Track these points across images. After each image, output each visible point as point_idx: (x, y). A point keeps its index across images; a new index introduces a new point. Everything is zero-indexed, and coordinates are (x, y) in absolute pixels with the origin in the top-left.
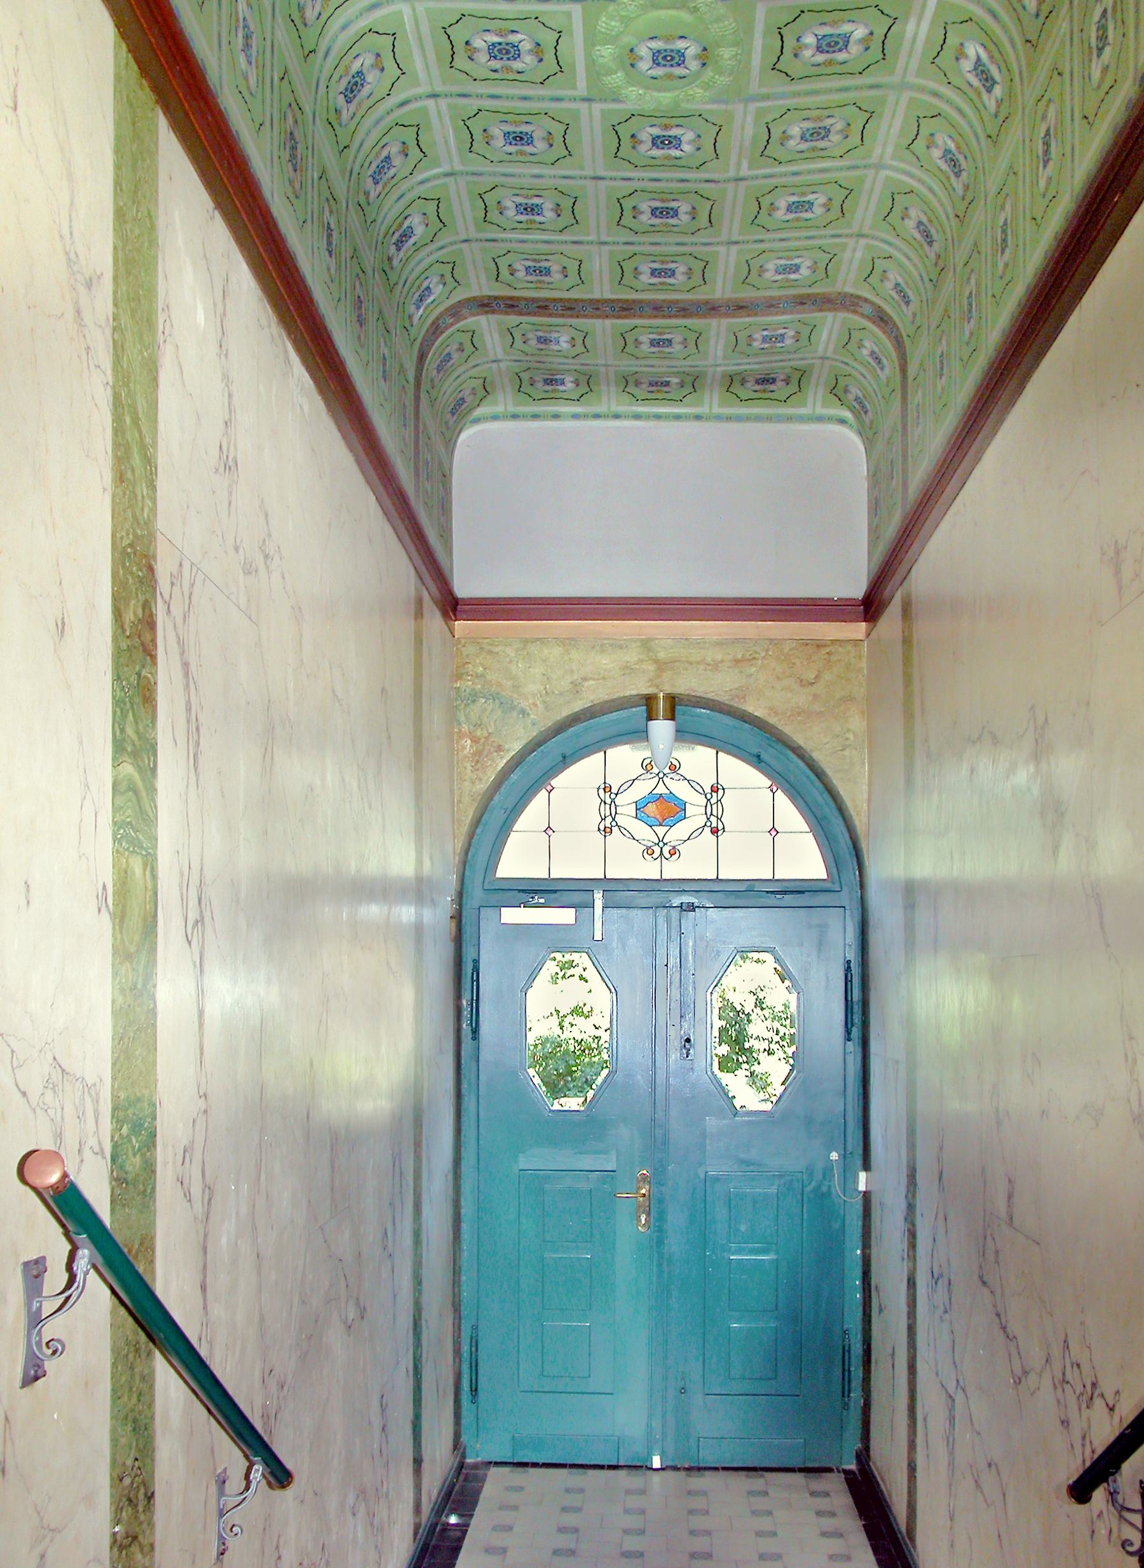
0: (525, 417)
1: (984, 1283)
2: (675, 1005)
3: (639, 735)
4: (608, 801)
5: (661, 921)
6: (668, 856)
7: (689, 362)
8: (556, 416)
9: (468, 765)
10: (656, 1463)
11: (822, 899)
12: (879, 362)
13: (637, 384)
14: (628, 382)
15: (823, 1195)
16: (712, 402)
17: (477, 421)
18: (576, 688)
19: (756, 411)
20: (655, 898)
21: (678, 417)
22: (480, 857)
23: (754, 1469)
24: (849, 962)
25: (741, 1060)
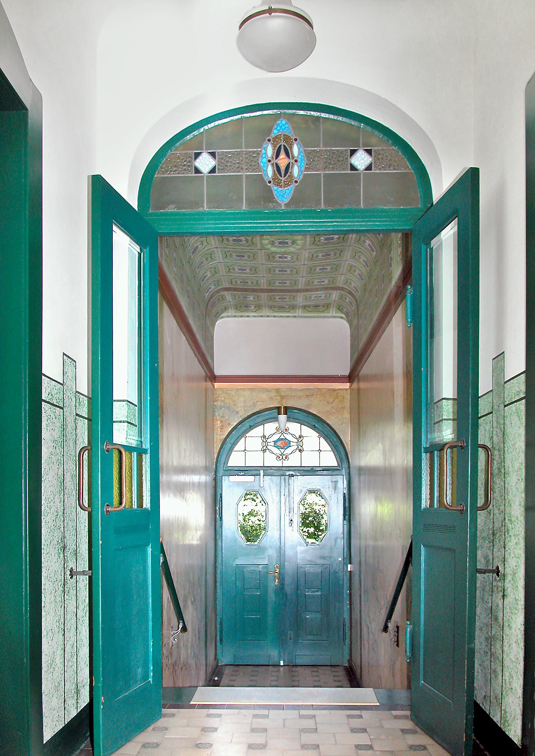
0: (238, 316)
1: (374, 589)
2: (287, 509)
3: (276, 419)
4: (265, 441)
5: (282, 480)
6: (285, 459)
7: (291, 303)
8: (248, 316)
9: (219, 430)
10: (282, 663)
11: (336, 472)
12: (351, 304)
13: (275, 307)
14: (271, 307)
15: (336, 572)
16: (299, 312)
17: (222, 317)
18: (254, 405)
19: (313, 315)
20: (281, 473)
21: (288, 317)
22: (223, 459)
23: (314, 665)
24: (345, 494)
25: (319, 534)
